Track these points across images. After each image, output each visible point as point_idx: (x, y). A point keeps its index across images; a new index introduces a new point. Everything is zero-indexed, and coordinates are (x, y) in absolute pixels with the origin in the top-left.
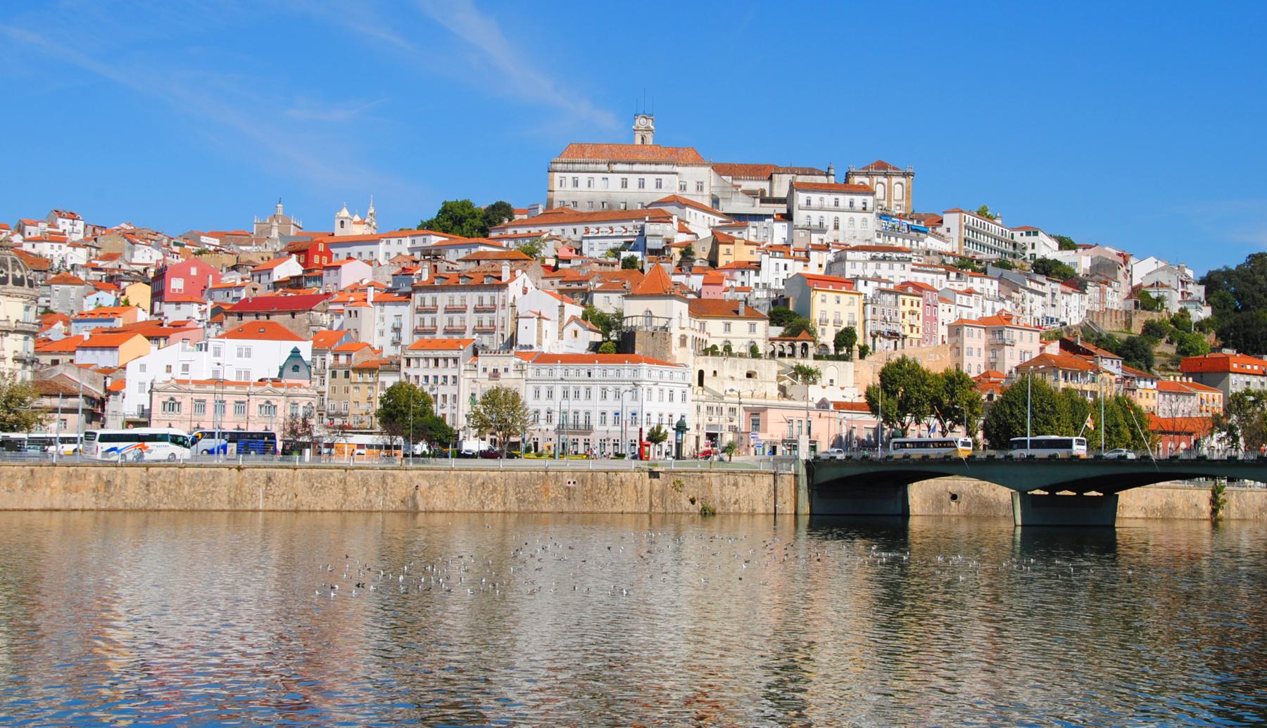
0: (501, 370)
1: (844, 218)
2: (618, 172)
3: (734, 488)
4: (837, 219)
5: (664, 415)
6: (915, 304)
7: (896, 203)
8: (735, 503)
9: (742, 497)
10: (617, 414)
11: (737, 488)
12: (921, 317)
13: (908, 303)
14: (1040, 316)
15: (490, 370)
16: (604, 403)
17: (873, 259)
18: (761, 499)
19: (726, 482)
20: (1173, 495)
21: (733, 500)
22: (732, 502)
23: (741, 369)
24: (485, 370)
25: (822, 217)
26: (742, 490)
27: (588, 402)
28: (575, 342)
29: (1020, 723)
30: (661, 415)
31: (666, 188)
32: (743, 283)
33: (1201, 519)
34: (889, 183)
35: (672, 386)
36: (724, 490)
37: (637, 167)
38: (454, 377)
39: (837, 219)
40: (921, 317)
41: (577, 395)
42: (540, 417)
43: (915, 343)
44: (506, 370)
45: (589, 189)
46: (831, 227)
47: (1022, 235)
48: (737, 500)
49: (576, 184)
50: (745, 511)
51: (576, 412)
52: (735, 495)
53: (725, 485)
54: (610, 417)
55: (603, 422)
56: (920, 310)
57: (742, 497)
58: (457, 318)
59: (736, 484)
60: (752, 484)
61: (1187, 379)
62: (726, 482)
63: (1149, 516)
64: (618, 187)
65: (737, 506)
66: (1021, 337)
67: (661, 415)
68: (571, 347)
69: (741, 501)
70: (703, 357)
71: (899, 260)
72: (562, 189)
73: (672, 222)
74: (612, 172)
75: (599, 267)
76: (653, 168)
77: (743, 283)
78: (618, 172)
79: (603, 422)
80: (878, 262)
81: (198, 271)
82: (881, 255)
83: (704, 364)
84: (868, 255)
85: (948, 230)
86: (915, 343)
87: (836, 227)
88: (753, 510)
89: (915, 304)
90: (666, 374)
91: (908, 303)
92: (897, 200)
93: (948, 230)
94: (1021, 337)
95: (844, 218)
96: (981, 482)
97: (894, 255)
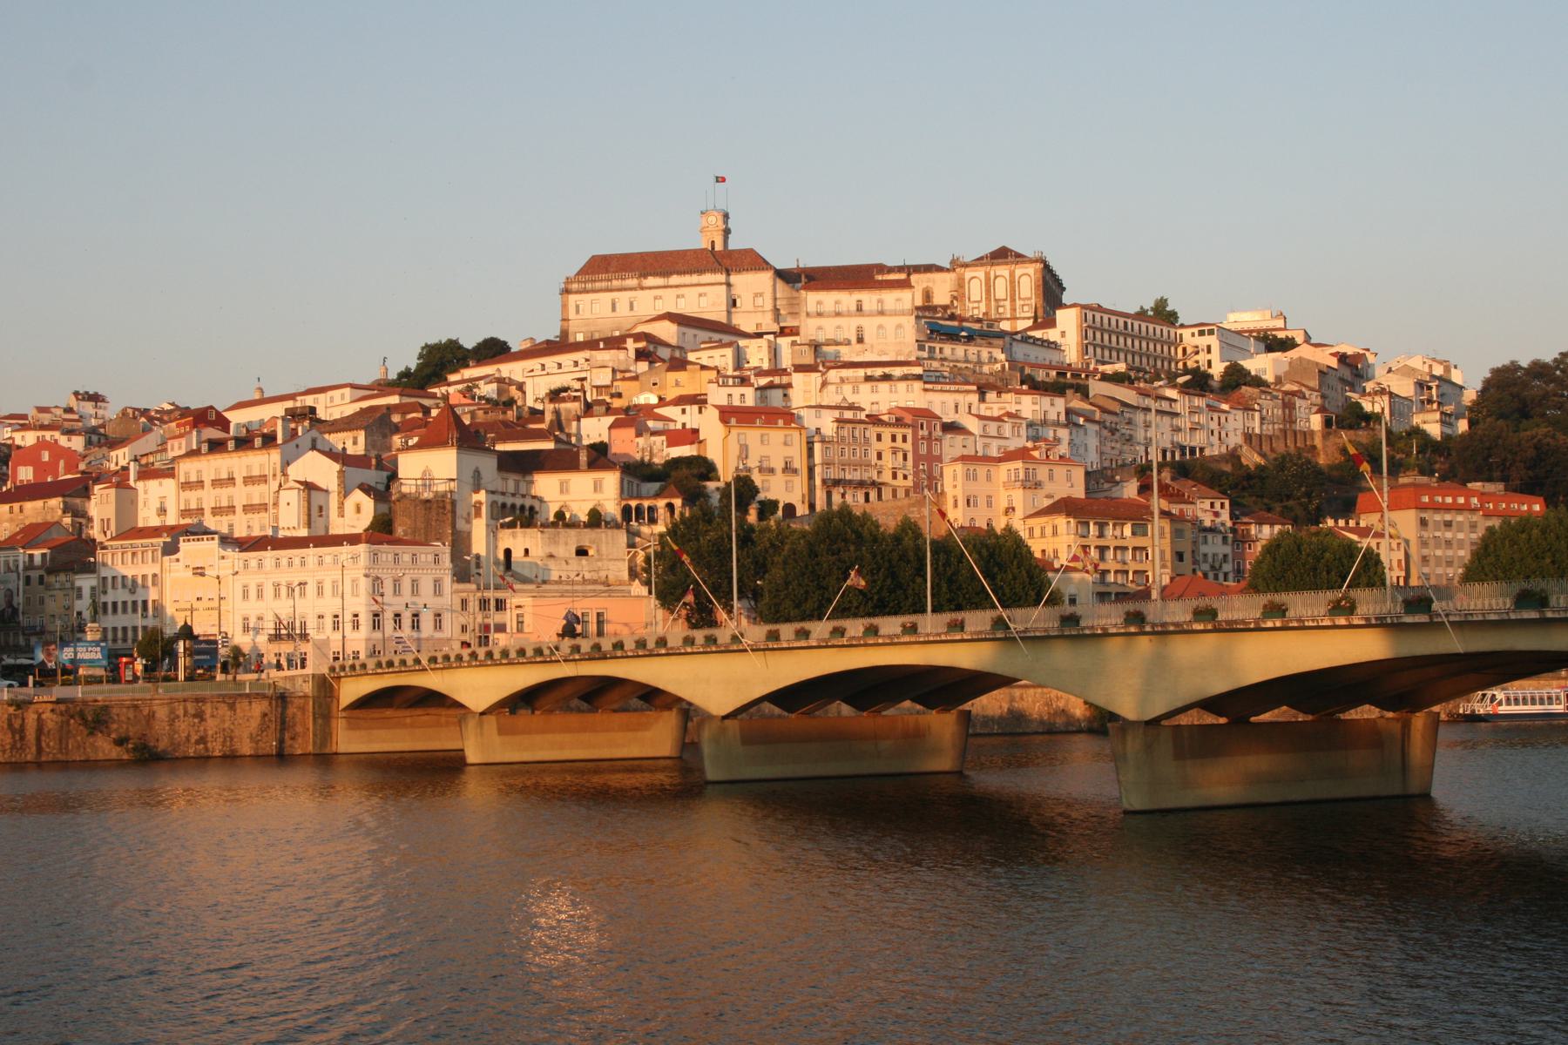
1: (869, 325)
2: (650, 288)
4: (860, 329)
6: (899, 438)
7: (1022, 302)
8: (197, 742)
10: (336, 616)
11: (202, 719)
12: (910, 456)
13: (887, 437)
17: (868, 379)
18: (246, 735)
19: (181, 712)
20: (1022, 698)
21: (194, 738)
22: (193, 741)
23: (566, 544)
27: (260, 603)
28: (358, 519)
29: (987, 1040)
33: (177, 758)
34: (1012, 274)
36: (177, 724)
38: (155, 576)
39: (860, 329)
40: (910, 456)
41: (260, 595)
43: (900, 494)
45: (613, 315)
47: (1193, 335)
50: (217, 753)
54: (329, 621)
57: (210, 733)
61: (1336, 522)
63: (978, 731)
64: (607, 312)
66: (1051, 477)
68: (353, 527)
69: (209, 739)
71: (905, 378)
72: (578, 317)
74: (642, 288)
76: (695, 278)
77: (684, 425)
78: (650, 288)
80: (874, 384)
81: (50, 456)
82: (878, 372)
83: (511, 539)
85: (1063, 334)
86: (900, 494)
89: (899, 438)
90: (253, 563)
91: (887, 437)
92: (1024, 299)
93: (1063, 334)
94: (1051, 477)
95: (869, 325)
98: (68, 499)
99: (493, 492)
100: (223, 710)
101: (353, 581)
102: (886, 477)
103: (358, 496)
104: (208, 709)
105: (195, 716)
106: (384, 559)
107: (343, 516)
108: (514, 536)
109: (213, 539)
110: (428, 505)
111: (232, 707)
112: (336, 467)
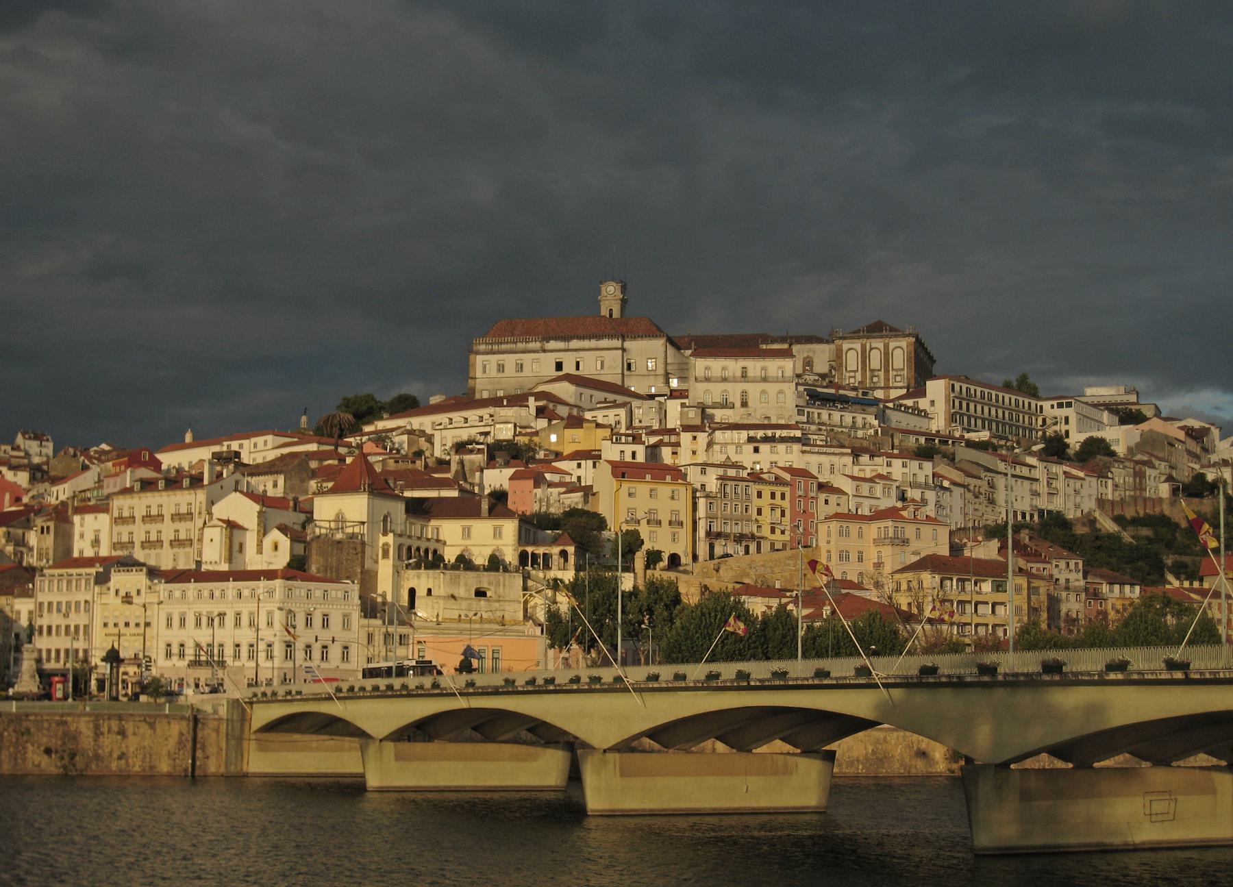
0: (134, 593)
1: (753, 390)
3: (119, 737)
4: (744, 393)
5: (187, 645)
6: (778, 496)
8: (120, 758)
9: (132, 749)
10: (252, 646)
14: (1027, 509)
15: (122, 593)
16: (169, 632)
18: (164, 752)
21: (115, 755)
24: (117, 592)
25: (725, 391)
26: (132, 743)
27: (182, 631)
28: (275, 556)
30: (238, 646)
31: (610, 367)
32: (579, 478)
34: (886, 347)
35: (239, 606)
37: (575, 344)
39: (744, 393)
40: (788, 513)
42: (172, 652)
44: (139, 592)
46: (738, 404)
47: (1052, 407)
48: (123, 754)
49: (501, 368)
51: (221, 645)
52: (120, 747)
53: (102, 733)
55: (237, 656)
56: (786, 504)
57: (132, 749)
58: (153, 528)
59: (122, 733)
60: (149, 732)
62: (105, 729)
65: (123, 761)
66: (918, 536)
67: (169, 645)
69: (130, 754)
70: (415, 571)
73: (528, 406)
74: (544, 351)
75: (395, 465)
76: (593, 343)
77: (579, 478)
78: (552, 351)
79: (237, 656)
84: (744, 435)
85: (932, 403)
87: (744, 404)
88: (152, 768)
89: (778, 496)
93: (932, 403)
94: (918, 536)
95: (753, 390)
96: (840, 741)
97: (778, 433)
98: (11, 530)
99: (400, 536)
100: (144, 729)
101: (344, 616)
102: (766, 531)
103: (275, 535)
104: (129, 727)
105: (119, 733)
106: (298, 594)
107: (261, 553)
108: (419, 577)
109: (141, 570)
110: (340, 545)
111: (152, 726)
112: (257, 507)
